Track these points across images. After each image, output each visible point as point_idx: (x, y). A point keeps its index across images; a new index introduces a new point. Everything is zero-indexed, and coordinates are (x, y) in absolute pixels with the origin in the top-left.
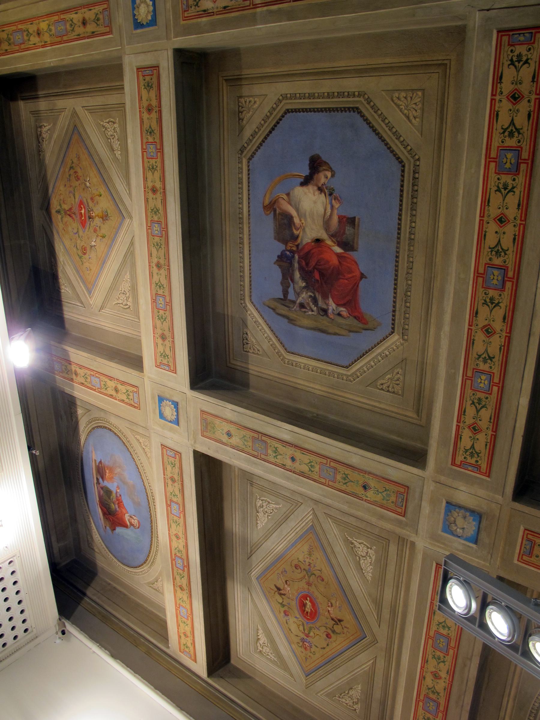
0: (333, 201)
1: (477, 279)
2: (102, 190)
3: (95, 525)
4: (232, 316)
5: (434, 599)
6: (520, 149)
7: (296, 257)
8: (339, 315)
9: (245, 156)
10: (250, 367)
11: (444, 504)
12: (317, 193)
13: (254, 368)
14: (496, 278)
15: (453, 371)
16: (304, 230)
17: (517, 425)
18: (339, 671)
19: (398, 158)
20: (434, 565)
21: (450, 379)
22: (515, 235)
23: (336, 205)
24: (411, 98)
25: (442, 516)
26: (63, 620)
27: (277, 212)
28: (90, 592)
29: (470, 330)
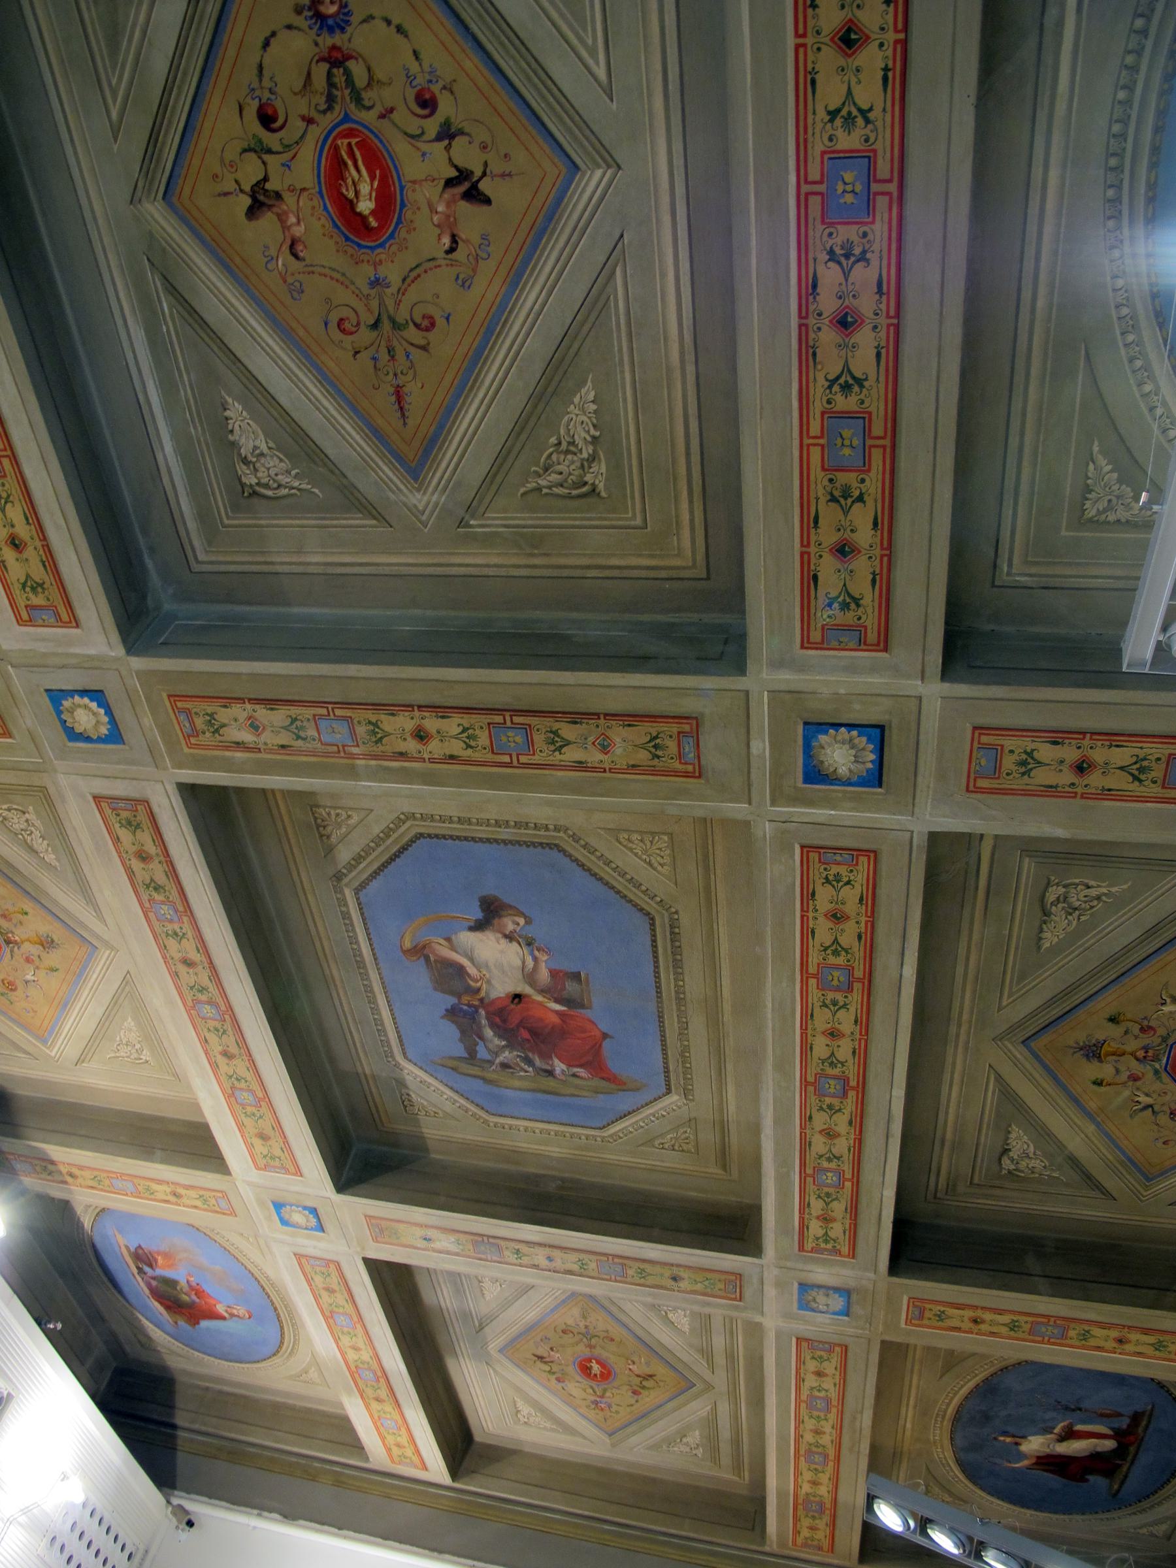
0: (536, 953)
1: (806, 200)
2: (28, 905)
3: (151, 1322)
4: (373, 1076)
5: (809, 543)
6: (871, 154)
7: (482, 1012)
8: (574, 1075)
9: (346, 885)
10: (424, 1130)
11: (796, 1285)
12: (503, 941)
13: (431, 1131)
14: (847, 442)
15: (785, 1170)
16: (489, 982)
17: (884, 1213)
18: (661, 1423)
19: (641, 910)
20: (794, 1340)
21: (782, 1180)
22: (874, 573)
23: (543, 957)
24: (651, 842)
25: (795, 1297)
26: (175, 1501)
27: (432, 959)
28: (181, 1419)
29: (803, 328)
